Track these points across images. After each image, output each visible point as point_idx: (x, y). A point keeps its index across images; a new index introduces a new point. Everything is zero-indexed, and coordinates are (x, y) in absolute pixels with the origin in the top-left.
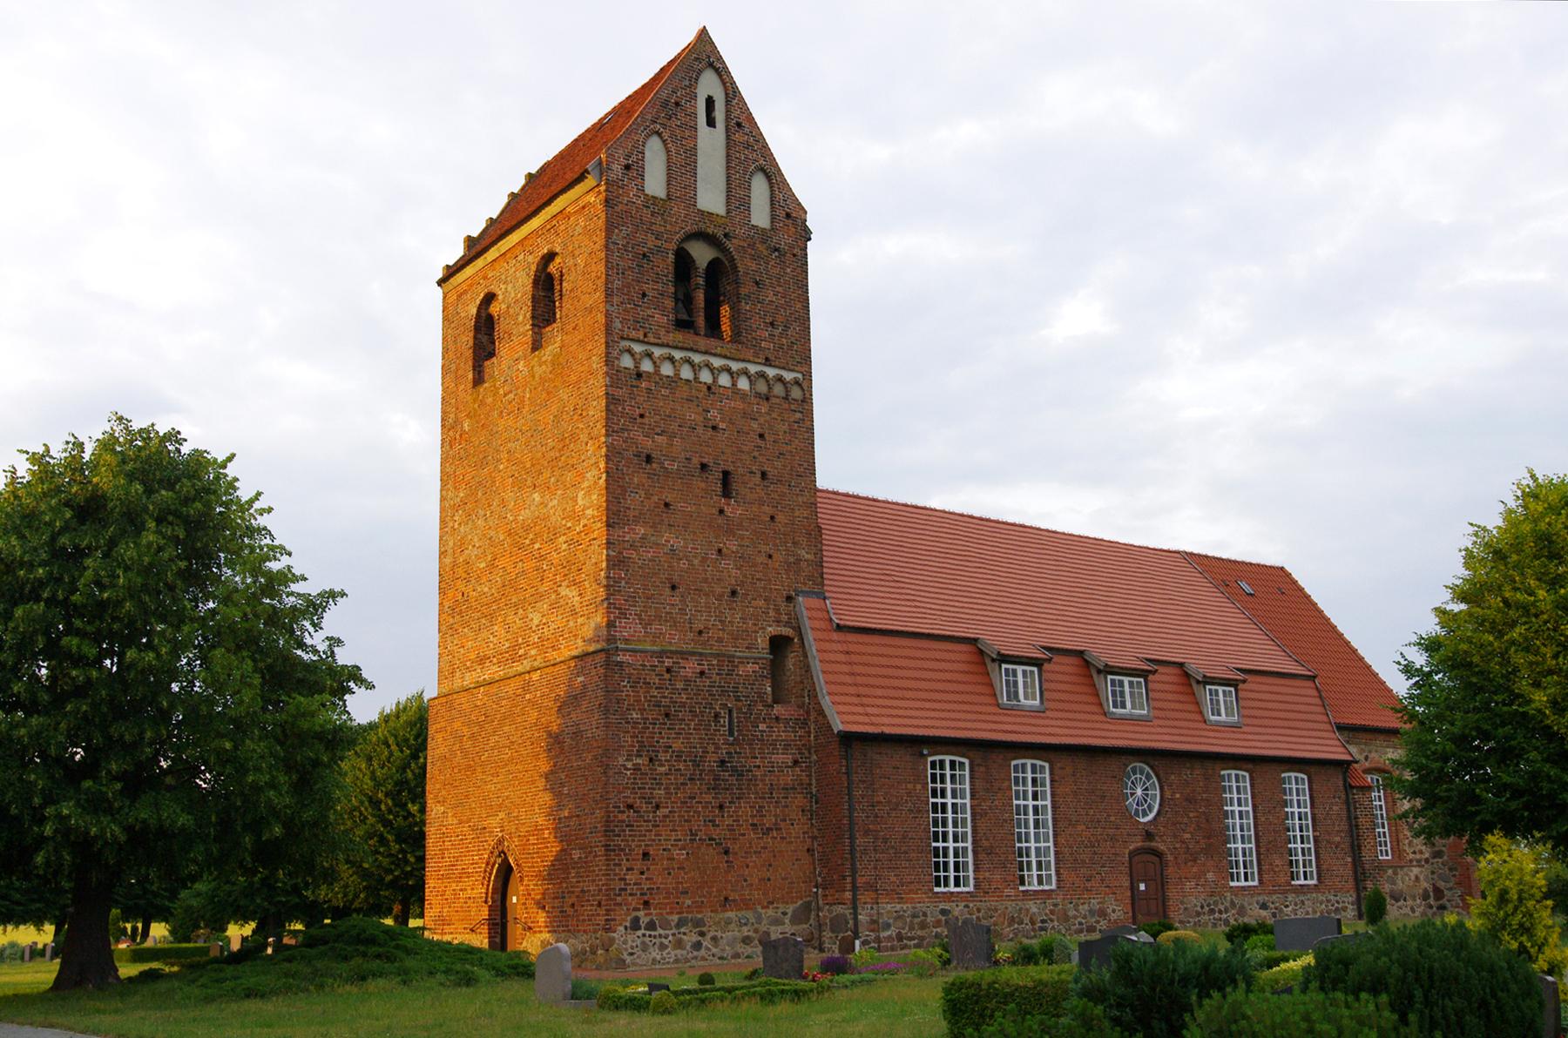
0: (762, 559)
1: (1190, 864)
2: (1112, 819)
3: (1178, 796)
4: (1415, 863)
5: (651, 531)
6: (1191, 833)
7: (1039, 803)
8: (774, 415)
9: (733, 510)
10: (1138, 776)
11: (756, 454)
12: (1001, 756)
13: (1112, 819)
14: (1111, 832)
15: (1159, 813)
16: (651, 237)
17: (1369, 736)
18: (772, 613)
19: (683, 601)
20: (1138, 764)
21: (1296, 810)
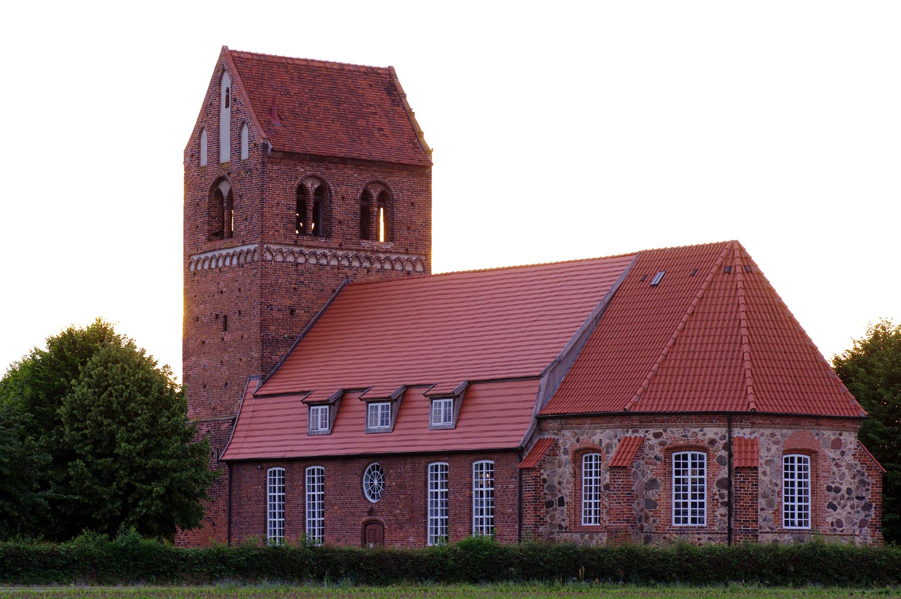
0: (237, 362)
1: (398, 531)
3: (394, 484)
6: (400, 509)
9: (228, 337)
10: (376, 472)
12: (298, 466)
15: (366, 499)
17: (578, 421)
21: (277, 520)
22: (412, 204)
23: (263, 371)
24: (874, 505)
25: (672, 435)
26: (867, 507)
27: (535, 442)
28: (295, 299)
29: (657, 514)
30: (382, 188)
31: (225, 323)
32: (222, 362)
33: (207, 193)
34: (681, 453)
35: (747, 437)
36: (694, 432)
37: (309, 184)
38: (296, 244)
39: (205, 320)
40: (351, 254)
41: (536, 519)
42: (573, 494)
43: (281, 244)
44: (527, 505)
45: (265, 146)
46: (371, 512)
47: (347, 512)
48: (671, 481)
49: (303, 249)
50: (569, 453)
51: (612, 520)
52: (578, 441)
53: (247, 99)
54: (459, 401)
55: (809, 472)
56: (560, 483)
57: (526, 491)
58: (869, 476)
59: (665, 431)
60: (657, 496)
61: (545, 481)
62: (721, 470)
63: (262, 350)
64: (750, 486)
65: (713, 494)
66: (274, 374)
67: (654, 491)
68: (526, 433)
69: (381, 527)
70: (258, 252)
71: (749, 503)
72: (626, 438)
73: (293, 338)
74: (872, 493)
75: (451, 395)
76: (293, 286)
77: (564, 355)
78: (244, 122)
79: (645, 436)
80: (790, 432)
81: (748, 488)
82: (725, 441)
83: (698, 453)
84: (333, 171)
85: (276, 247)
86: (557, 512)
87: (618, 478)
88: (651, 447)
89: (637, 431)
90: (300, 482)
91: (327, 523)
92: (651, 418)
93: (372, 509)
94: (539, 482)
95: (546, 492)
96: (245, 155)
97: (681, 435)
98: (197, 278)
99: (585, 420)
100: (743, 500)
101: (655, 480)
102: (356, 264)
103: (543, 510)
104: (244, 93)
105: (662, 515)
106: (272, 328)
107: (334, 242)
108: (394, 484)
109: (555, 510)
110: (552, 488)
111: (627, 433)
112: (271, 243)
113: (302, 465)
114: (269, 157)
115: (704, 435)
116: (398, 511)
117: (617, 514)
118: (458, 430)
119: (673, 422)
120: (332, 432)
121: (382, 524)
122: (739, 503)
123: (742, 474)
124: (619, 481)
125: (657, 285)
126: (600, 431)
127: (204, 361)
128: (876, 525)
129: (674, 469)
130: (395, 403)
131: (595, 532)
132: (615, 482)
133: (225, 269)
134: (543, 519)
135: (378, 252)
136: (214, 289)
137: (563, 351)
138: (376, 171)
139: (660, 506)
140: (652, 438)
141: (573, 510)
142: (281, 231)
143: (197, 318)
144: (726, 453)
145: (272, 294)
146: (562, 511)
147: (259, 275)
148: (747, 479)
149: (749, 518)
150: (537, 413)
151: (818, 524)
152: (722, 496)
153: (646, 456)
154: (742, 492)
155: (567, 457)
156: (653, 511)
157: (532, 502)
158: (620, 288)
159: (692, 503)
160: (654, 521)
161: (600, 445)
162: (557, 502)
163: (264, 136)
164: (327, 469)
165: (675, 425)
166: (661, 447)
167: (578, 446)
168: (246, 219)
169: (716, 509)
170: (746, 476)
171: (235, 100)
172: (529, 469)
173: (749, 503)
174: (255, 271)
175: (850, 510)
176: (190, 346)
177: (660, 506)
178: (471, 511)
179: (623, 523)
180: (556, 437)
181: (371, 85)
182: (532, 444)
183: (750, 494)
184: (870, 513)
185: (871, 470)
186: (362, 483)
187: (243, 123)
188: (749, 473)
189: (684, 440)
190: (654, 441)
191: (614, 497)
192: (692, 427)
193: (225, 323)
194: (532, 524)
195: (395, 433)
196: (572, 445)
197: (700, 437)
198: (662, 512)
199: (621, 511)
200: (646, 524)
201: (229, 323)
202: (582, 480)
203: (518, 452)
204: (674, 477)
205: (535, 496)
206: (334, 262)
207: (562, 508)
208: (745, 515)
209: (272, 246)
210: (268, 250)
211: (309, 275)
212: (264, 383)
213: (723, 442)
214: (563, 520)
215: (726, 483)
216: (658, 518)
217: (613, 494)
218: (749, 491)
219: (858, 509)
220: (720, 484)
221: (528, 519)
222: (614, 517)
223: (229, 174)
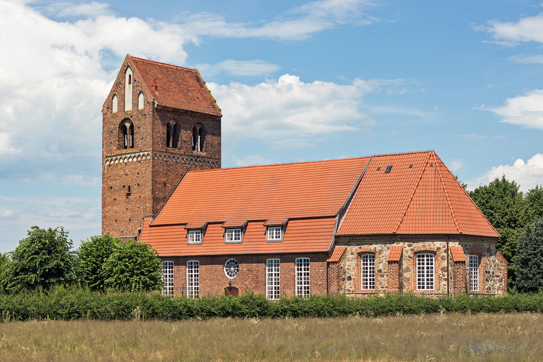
0: (137, 209)
2: (219, 278)
3: (245, 269)
4: (382, 292)
5: (111, 207)
7: (190, 274)
8: (142, 166)
11: (137, 179)
13: (219, 278)
14: (218, 282)
15: (226, 276)
16: (113, 126)
18: (139, 224)
19: (118, 224)
20: (232, 259)
24: (504, 279)
32: (127, 209)
42: (357, 274)
47: (214, 283)
50: (355, 254)
53: (142, 80)
55: (362, 282)
61: (342, 268)
63: (153, 203)
67: (408, 273)
71: (461, 279)
74: (503, 274)
76: (165, 172)
78: (141, 91)
80: (472, 244)
82: (445, 248)
86: (347, 283)
87: (392, 267)
96: (141, 106)
97: (422, 245)
98: (111, 168)
100: (458, 277)
103: (341, 282)
109: (346, 282)
116: (248, 283)
122: (457, 279)
136: (122, 173)
143: (111, 187)
144: (446, 254)
146: (350, 283)
147: (151, 166)
152: (444, 275)
164: (201, 261)
167: (360, 251)
168: (142, 138)
171: (135, 80)
173: (461, 279)
174: (148, 164)
175: (493, 282)
181: (190, 77)
183: (462, 274)
190: (408, 248)
197: (432, 246)
204: (417, 266)
211: (172, 167)
212: (154, 219)
213: (444, 249)
214: (351, 287)
215: (446, 269)
220: (443, 269)
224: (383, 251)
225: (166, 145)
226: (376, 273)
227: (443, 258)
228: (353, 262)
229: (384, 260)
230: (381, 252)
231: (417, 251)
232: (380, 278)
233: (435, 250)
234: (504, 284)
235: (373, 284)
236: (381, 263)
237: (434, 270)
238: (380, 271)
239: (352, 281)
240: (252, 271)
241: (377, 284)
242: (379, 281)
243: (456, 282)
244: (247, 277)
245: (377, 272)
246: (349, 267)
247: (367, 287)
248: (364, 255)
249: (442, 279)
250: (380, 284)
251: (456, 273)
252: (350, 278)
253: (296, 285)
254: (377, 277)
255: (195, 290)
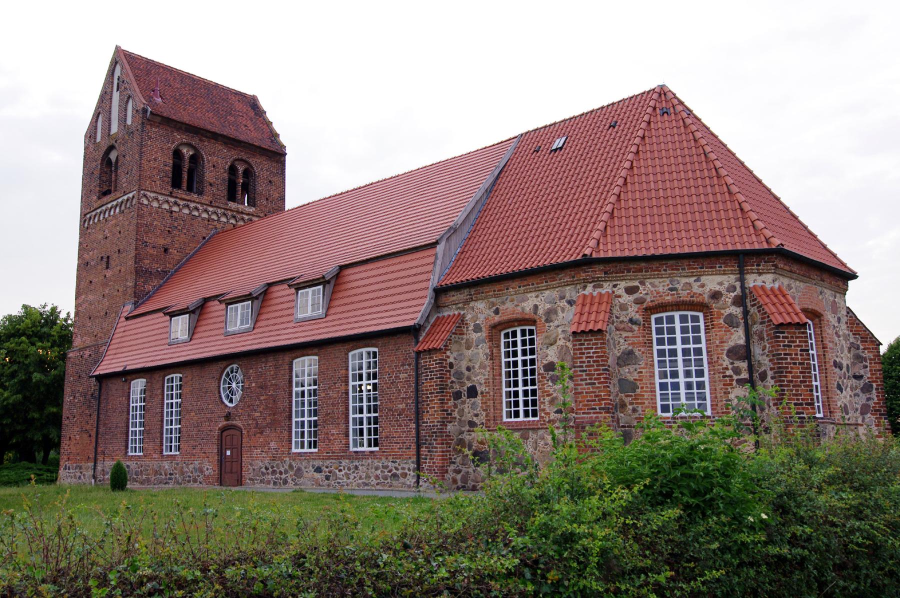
0: (116, 293)
3: (254, 385)
9: (109, 273)
14: (209, 416)
15: (223, 403)
22: (270, 182)
23: (135, 297)
24: (874, 385)
25: (653, 289)
26: (867, 389)
27: (432, 320)
28: (169, 240)
29: (638, 399)
30: (247, 166)
31: (108, 263)
33: (99, 162)
34: (664, 315)
35: (768, 286)
36: (687, 283)
37: (185, 150)
38: (171, 195)
39: (93, 263)
40: (219, 211)
41: (444, 414)
42: (491, 381)
43: (157, 193)
44: (428, 397)
45: (145, 111)
46: (228, 417)
48: (652, 354)
49: (177, 200)
50: (484, 329)
51: (581, 409)
52: (497, 312)
54: (329, 288)
55: (504, 400)
56: (468, 369)
57: (426, 379)
58: (864, 349)
59: (642, 283)
60: (635, 373)
61: (451, 365)
62: (732, 334)
63: (136, 280)
64: (799, 353)
65: (723, 369)
66: (147, 300)
67: (632, 369)
68: (423, 308)
69: (238, 433)
70: (136, 197)
71: (798, 377)
72: (585, 296)
73: (166, 272)
74: (871, 371)
75: (321, 280)
77: (459, 223)
79: (613, 292)
81: (796, 354)
82: (735, 293)
83: (689, 313)
84: (206, 144)
85: (153, 195)
86: (466, 405)
88: (623, 307)
89: (601, 286)
90: (160, 391)
91: (184, 430)
92: (622, 266)
93: (230, 414)
94: (445, 367)
95: (453, 379)
96: (129, 122)
97: (666, 288)
99: (507, 284)
100: (790, 372)
101: (631, 353)
102: (224, 219)
103: (451, 403)
104: (131, 74)
105: (646, 402)
106: (147, 261)
107: (205, 199)
108: (254, 385)
109: (464, 402)
110: (459, 375)
111: (584, 290)
112: (148, 191)
113: (162, 374)
114: (149, 120)
115: (703, 286)
116: (258, 414)
117: (588, 401)
118: (329, 318)
119: (655, 271)
120: (191, 340)
121: (239, 429)
122: (786, 377)
123: (786, 335)
124: (589, 353)
125: (561, 148)
126: (533, 294)
127: (91, 297)
128: (880, 411)
129: (655, 336)
130: (256, 302)
131: (533, 429)
132: (583, 354)
133: (110, 218)
134: (451, 414)
135: (242, 213)
136: (101, 237)
137: (459, 217)
138: (241, 151)
139: (642, 388)
140: (624, 294)
141: (492, 402)
142: (158, 182)
145: (146, 233)
146: (474, 403)
148: (793, 342)
149: (803, 399)
150: (435, 285)
151: (832, 410)
152: (737, 371)
153: (615, 320)
154: (789, 360)
155: (479, 334)
156: (631, 396)
157: (437, 393)
158: (508, 164)
159: (678, 377)
160: (634, 410)
161: (535, 313)
162: (466, 393)
163: (145, 102)
165: (658, 274)
166: (638, 306)
167: (497, 319)
169: (730, 390)
170: (792, 337)
172: (430, 351)
173: (798, 377)
176: (81, 287)
177: (642, 388)
178: (347, 409)
179: (601, 413)
180: (462, 313)
182: (429, 323)
183: (800, 364)
184: (871, 396)
185: (866, 342)
186: (219, 387)
187: (129, 97)
188: (795, 333)
189: (671, 295)
190: (626, 299)
191: (582, 375)
192: (684, 276)
193: (108, 263)
194: (438, 422)
195: (256, 331)
196: (488, 319)
197: (696, 289)
198: (645, 397)
199: (596, 396)
200: (622, 415)
201: (111, 262)
202: (501, 363)
203: (413, 331)
204: (656, 347)
205: (440, 385)
206: (205, 215)
207: (473, 400)
208: (796, 395)
209: (149, 194)
210: (145, 196)
213: (733, 294)
214: (476, 415)
215: (743, 351)
216: (640, 406)
217: (581, 371)
218: (798, 359)
219: (857, 391)
220: (733, 353)
221: (430, 415)
222: (583, 405)
223: (116, 142)
224: (556, 313)
225: (170, 184)
226: (539, 374)
227: (731, 321)
228: (481, 351)
229: (561, 336)
230: (550, 314)
231: (654, 304)
232: (550, 387)
233: (706, 298)
234: (876, 399)
235: (534, 403)
236: (551, 345)
237: (705, 357)
238: (550, 367)
239: (478, 399)
240: (266, 387)
241: (544, 404)
242: (548, 395)
243: (786, 386)
244: (258, 402)
245: (542, 371)
246: (471, 364)
247: (517, 414)
248: (506, 331)
249: (734, 383)
250: (552, 402)
251: (782, 359)
252: (472, 392)
253: (351, 416)
254: (543, 385)
255: (310, 427)
